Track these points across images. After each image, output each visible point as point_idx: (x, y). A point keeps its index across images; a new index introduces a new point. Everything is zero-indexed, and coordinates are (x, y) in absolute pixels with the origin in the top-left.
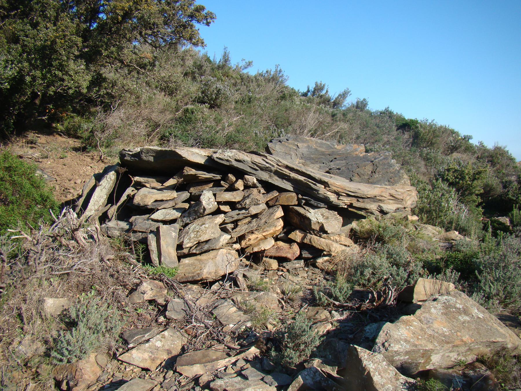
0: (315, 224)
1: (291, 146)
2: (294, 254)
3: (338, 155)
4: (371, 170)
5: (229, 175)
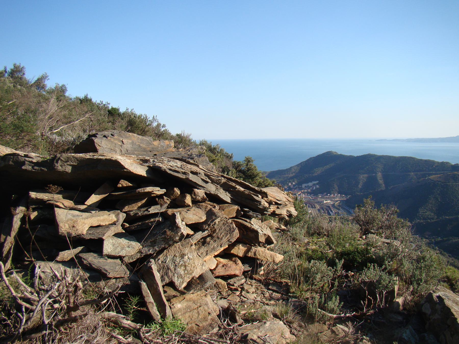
0: (261, 236)
1: (116, 142)
2: (240, 270)
5: (175, 189)
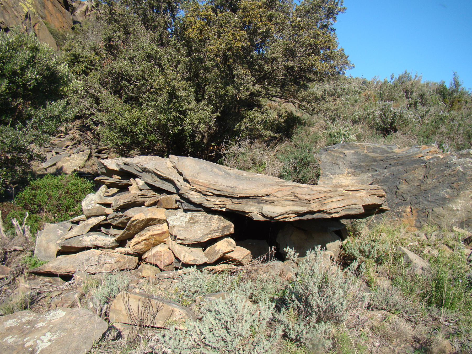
1: (337, 154)
3: (394, 159)
4: (423, 173)
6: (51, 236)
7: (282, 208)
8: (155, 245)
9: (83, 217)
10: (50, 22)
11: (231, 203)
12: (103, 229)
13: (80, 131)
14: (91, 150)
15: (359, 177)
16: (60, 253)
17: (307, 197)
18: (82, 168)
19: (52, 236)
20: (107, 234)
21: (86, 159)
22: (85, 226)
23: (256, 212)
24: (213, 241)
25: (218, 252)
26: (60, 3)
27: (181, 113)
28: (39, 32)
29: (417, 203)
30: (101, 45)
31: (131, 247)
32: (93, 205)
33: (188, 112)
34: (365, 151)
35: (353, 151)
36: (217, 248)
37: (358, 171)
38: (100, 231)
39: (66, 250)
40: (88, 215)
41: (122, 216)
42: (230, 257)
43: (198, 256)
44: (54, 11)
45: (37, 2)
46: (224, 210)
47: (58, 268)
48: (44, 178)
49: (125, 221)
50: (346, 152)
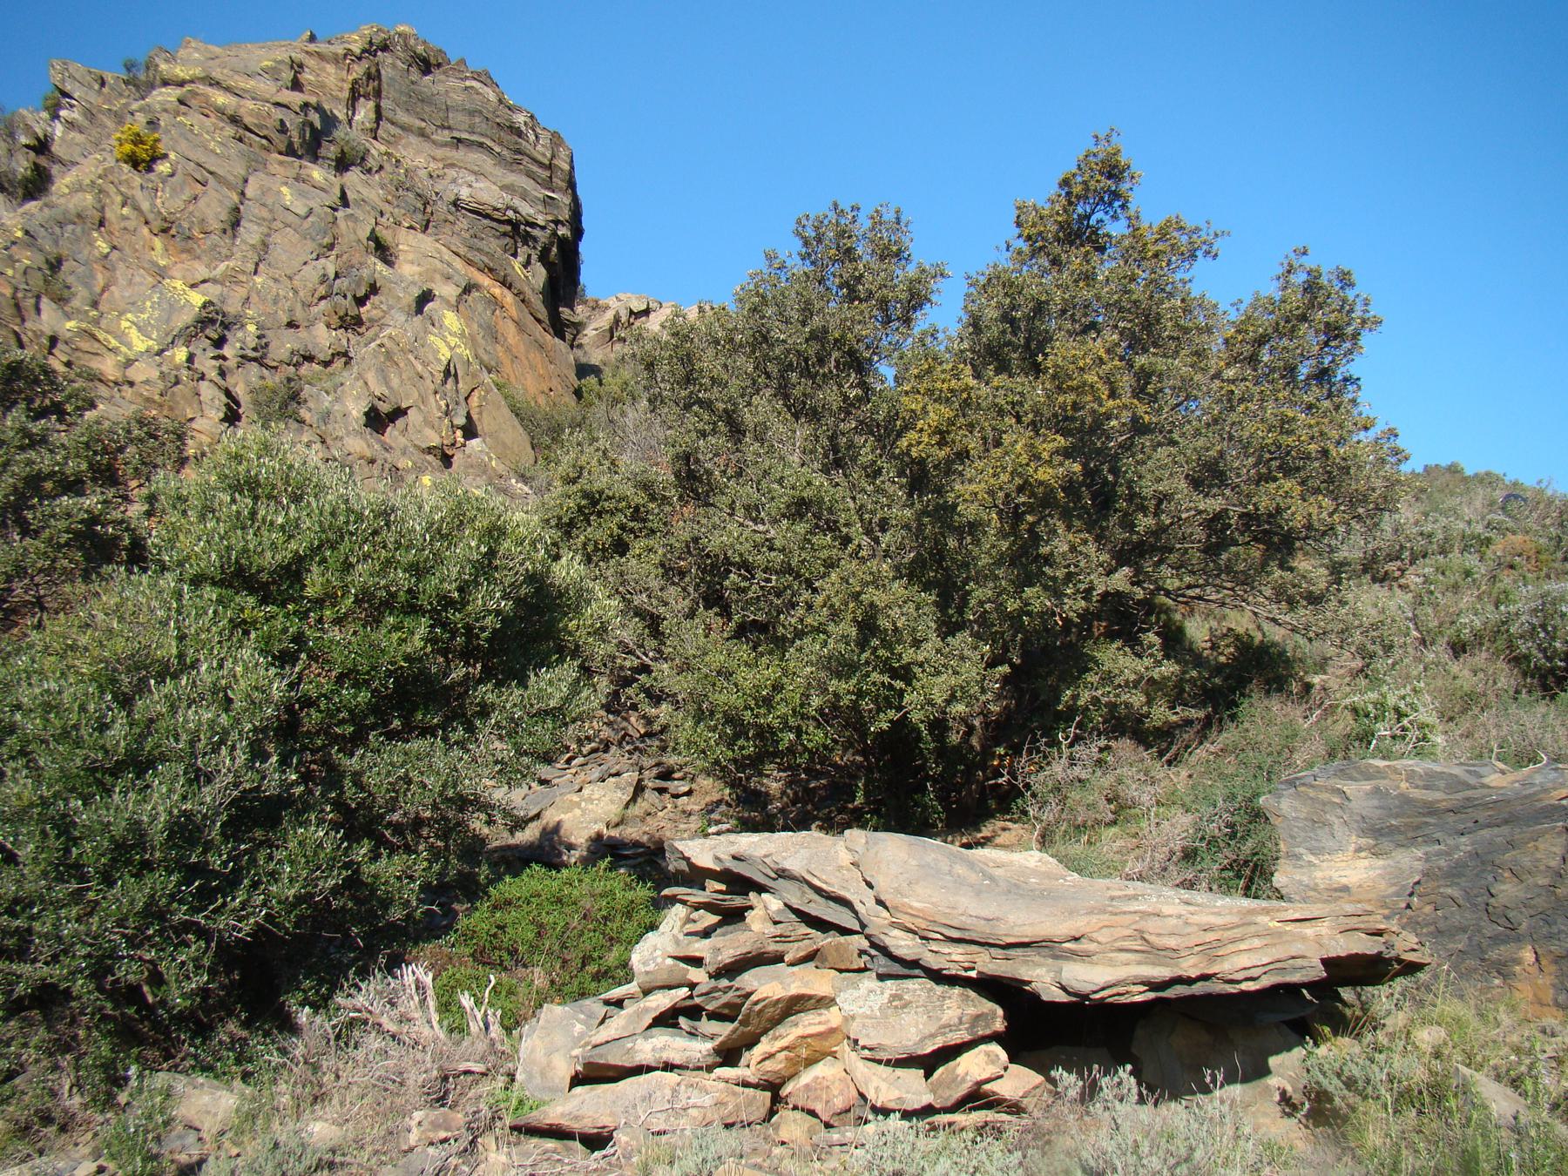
1: (1324, 796)
3: (1486, 806)
6: (555, 1039)
7: (1109, 970)
8: (810, 1062)
9: (632, 988)
10: (512, 379)
11: (987, 958)
12: (682, 1021)
13: (608, 711)
14: (641, 768)
15: (1390, 862)
16: (577, 1080)
17: (1172, 942)
18: (617, 825)
19: (559, 1039)
20: (692, 1034)
21: (626, 798)
22: (639, 1015)
23: (1048, 980)
24: (949, 1053)
25: (964, 1080)
26: (539, 321)
27: (894, 673)
28: (480, 413)
29: (1550, 937)
30: (664, 474)
31: (752, 1065)
32: (659, 960)
33: (917, 670)
34: (1404, 785)
35: (1367, 786)
36: (960, 1071)
37: (1386, 844)
38: (676, 1025)
39: (593, 1074)
40: (647, 986)
41: (730, 988)
42: (994, 1093)
43: (912, 1088)
44: (522, 348)
45: (475, 326)
46: (973, 974)
47: (576, 1117)
48: (524, 877)
49: (738, 1001)
50: (1349, 788)
